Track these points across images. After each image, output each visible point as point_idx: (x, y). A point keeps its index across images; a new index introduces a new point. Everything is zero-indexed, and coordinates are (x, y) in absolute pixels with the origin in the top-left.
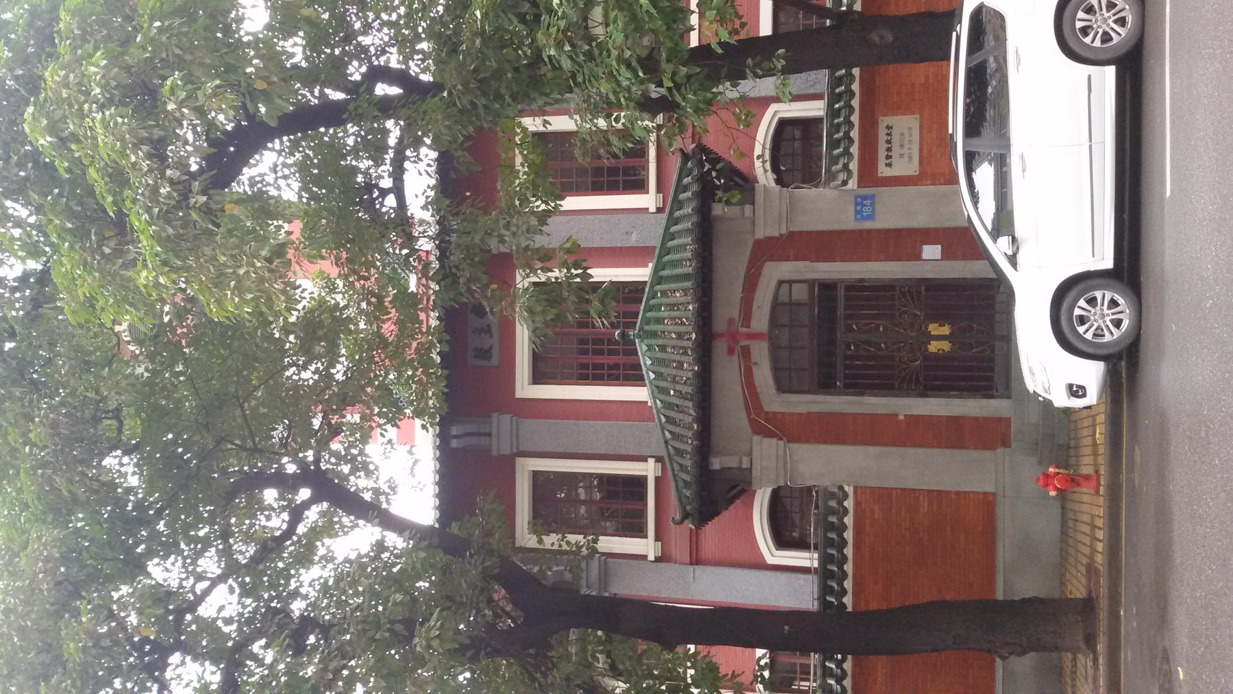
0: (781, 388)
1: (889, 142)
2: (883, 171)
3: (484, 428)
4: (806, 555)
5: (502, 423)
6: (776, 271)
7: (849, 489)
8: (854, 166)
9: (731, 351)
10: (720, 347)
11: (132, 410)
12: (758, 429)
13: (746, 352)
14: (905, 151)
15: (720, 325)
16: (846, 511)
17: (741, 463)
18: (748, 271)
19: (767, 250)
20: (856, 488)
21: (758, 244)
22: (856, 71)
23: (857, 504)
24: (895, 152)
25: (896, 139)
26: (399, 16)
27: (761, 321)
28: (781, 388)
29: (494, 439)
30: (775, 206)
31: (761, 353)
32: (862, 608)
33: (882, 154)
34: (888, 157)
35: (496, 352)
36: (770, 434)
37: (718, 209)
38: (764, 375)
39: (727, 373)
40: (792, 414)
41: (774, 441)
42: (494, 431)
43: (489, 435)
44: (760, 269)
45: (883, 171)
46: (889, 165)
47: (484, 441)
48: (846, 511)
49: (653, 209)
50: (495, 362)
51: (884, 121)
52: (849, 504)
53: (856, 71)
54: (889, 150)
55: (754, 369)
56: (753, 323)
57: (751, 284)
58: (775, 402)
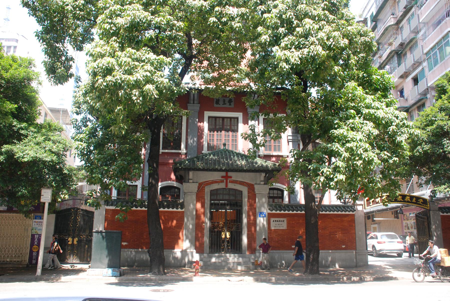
0: (241, 192)
1: (280, 221)
2: (272, 220)
3: (195, 102)
4: (116, 195)
5: (197, 107)
6: (245, 190)
7: (183, 210)
8: (274, 212)
9: (222, 177)
10: (224, 174)
11: (149, 19)
12: (200, 184)
13: (222, 181)
14: (277, 225)
15: (230, 174)
16: (177, 209)
17: (191, 179)
18: (245, 182)
19: (251, 188)
20: (184, 212)
21: (253, 185)
22: (303, 212)
23: (179, 212)
24: (277, 223)
25: (280, 223)
26: (286, 85)
27: (231, 186)
28: (241, 192)
29: (192, 105)
30: (262, 190)
31: (222, 186)
32: (160, 214)
33: (277, 219)
34: (276, 221)
35: (218, 106)
36: (199, 188)
37: (263, 175)
38: (215, 186)
39: (217, 176)
40: (204, 194)
41: (197, 189)
42: (195, 105)
43: (194, 103)
44: (246, 186)
45: (272, 220)
46: (274, 221)
47: (192, 102)
48: (177, 209)
49: (259, 154)
50: (215, 105)
51: (285, 220)
52: (179, 210)
53: (303, 212)
54: (278, 221)
55: (217, 184)
56: (230, 184)
57: (242, 183)
58: (207, 190)
